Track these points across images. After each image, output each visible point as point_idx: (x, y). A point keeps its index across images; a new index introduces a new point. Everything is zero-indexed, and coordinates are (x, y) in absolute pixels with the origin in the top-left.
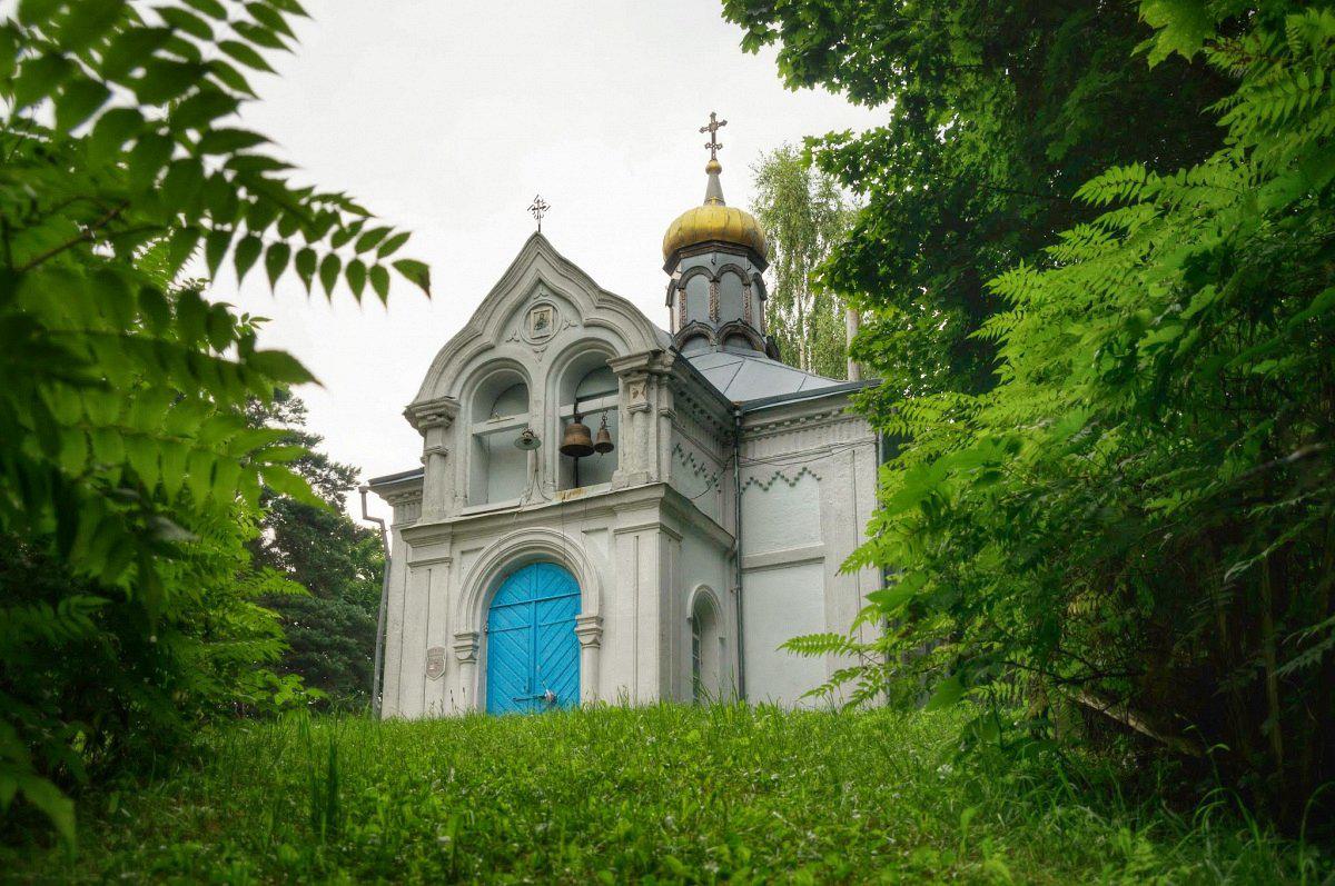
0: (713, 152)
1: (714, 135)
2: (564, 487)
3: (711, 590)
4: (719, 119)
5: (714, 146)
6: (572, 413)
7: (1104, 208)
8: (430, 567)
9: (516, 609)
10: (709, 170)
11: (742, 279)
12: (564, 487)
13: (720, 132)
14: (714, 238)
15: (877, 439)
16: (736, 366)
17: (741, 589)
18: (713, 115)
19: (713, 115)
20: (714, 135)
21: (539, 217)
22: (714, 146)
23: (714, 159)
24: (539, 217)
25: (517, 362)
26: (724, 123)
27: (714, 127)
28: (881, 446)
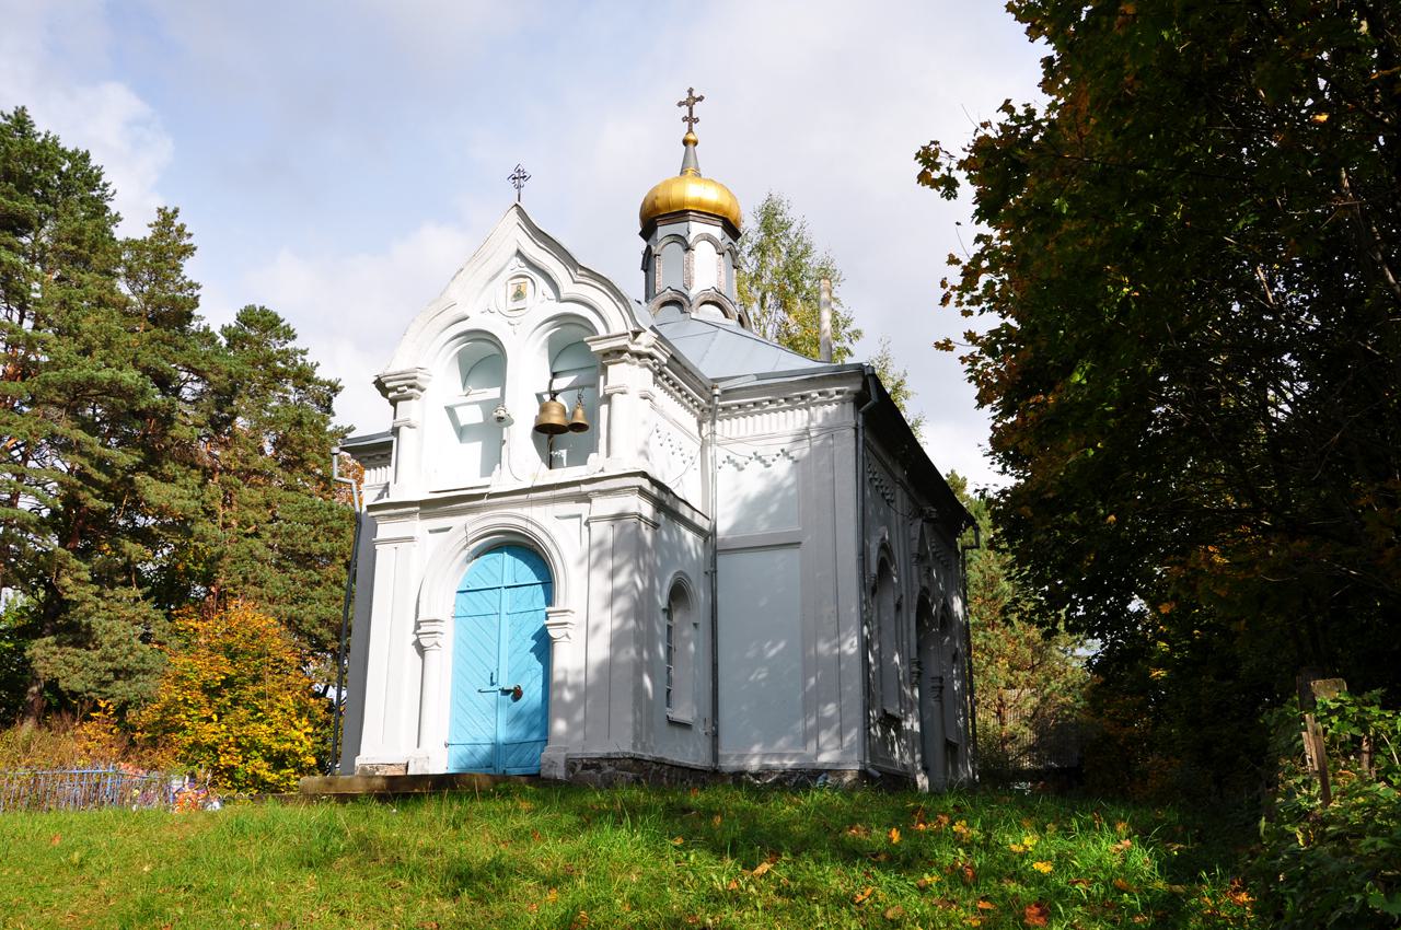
0: (690, 125)
1: (691, 109)
2: (482, 476)
3: (687, 577)
4: (696, 94)
5: (691, 120)
6: (546, 389)
7: (814, 380)
8: (396, 545)
9: (464, 613)
10: (686, 142)
11: (716, 248)
12: (482, 476)
13: (697, 107)
14: (690, 208)
15: (857, 425)
16: (710, 336)
17: (716, 572)
18: (690, 91)
19: (690, 91)
20: (691, 109)
21: (519, 187)
22: (691, 120)
23: (690, 131)
24: (519, 187)
25: (496, 338)
26: (701, 99)
27: (692, 100)
28: (860, 431)
